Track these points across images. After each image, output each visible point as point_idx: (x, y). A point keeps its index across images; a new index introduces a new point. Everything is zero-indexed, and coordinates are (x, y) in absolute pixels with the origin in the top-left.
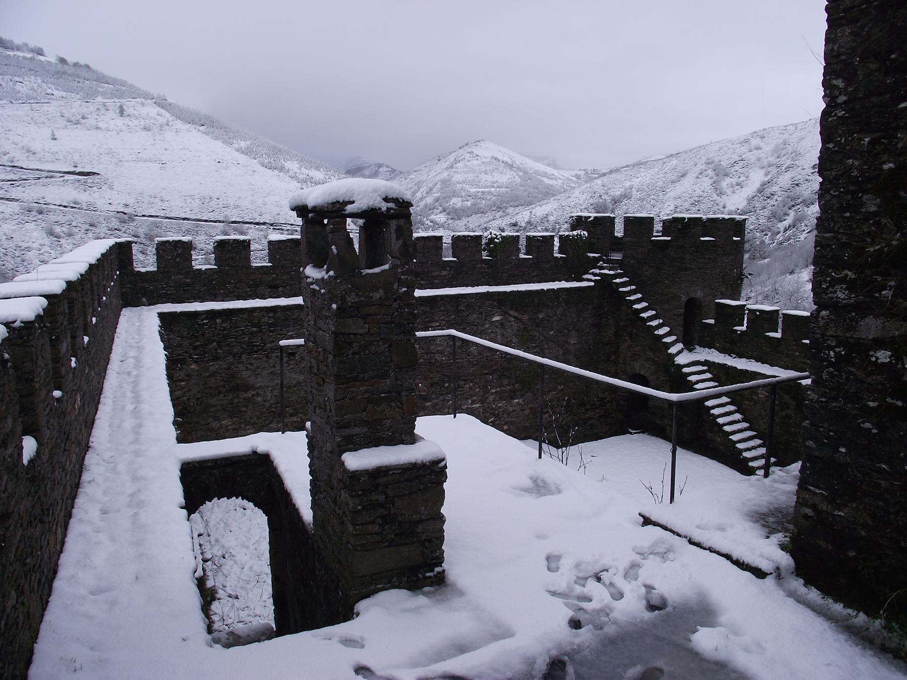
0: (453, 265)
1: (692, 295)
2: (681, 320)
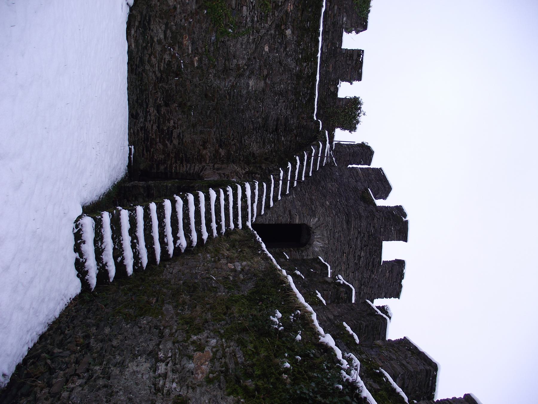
0: (137, 148)
1: (317, 235)
2: (285, 219)
